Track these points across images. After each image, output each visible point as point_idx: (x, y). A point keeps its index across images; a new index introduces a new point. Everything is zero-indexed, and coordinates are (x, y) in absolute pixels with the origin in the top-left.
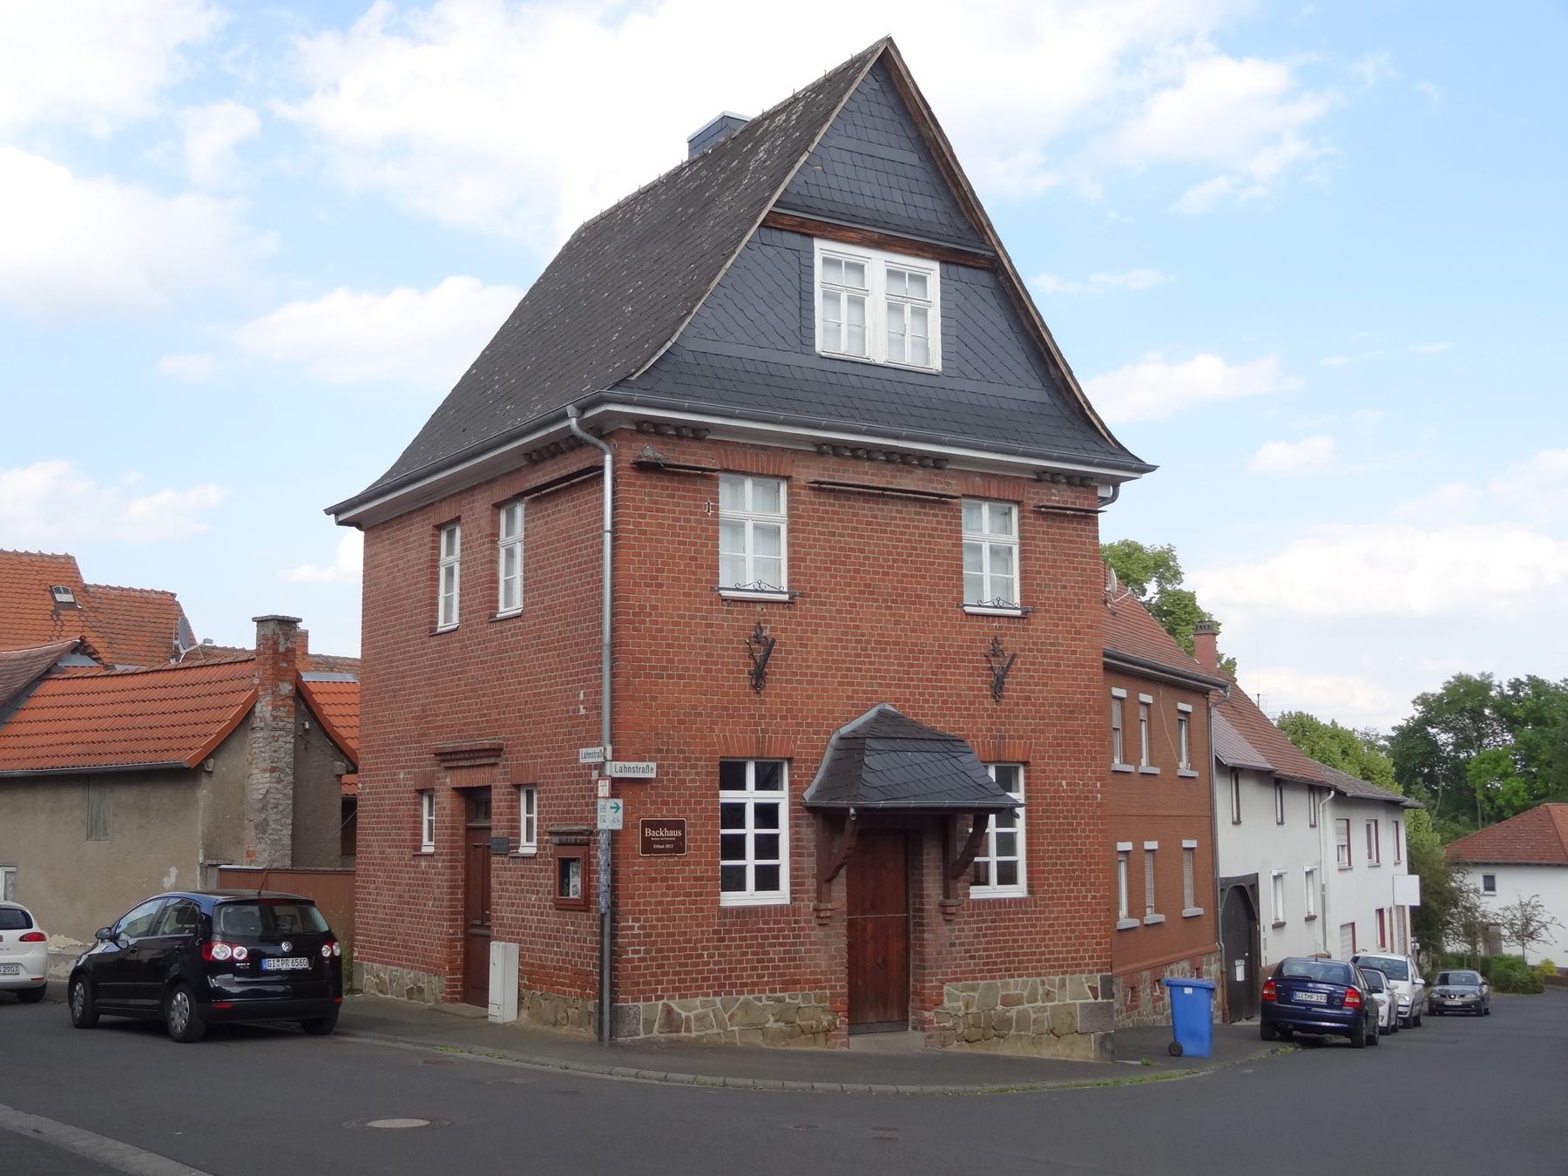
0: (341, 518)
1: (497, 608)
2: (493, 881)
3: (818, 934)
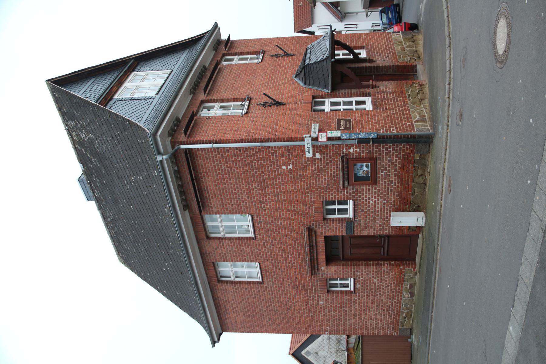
0: (216, 340)
1: (250, 238)
2: (365, 233)
3: (382, 88)
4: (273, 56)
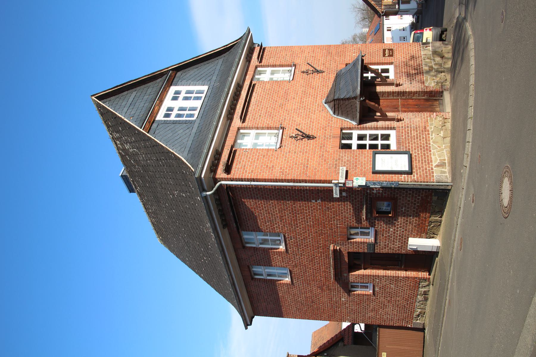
0: (249, 323)
2: (385, 251)
3: (406, 121)
4: (303, 72)
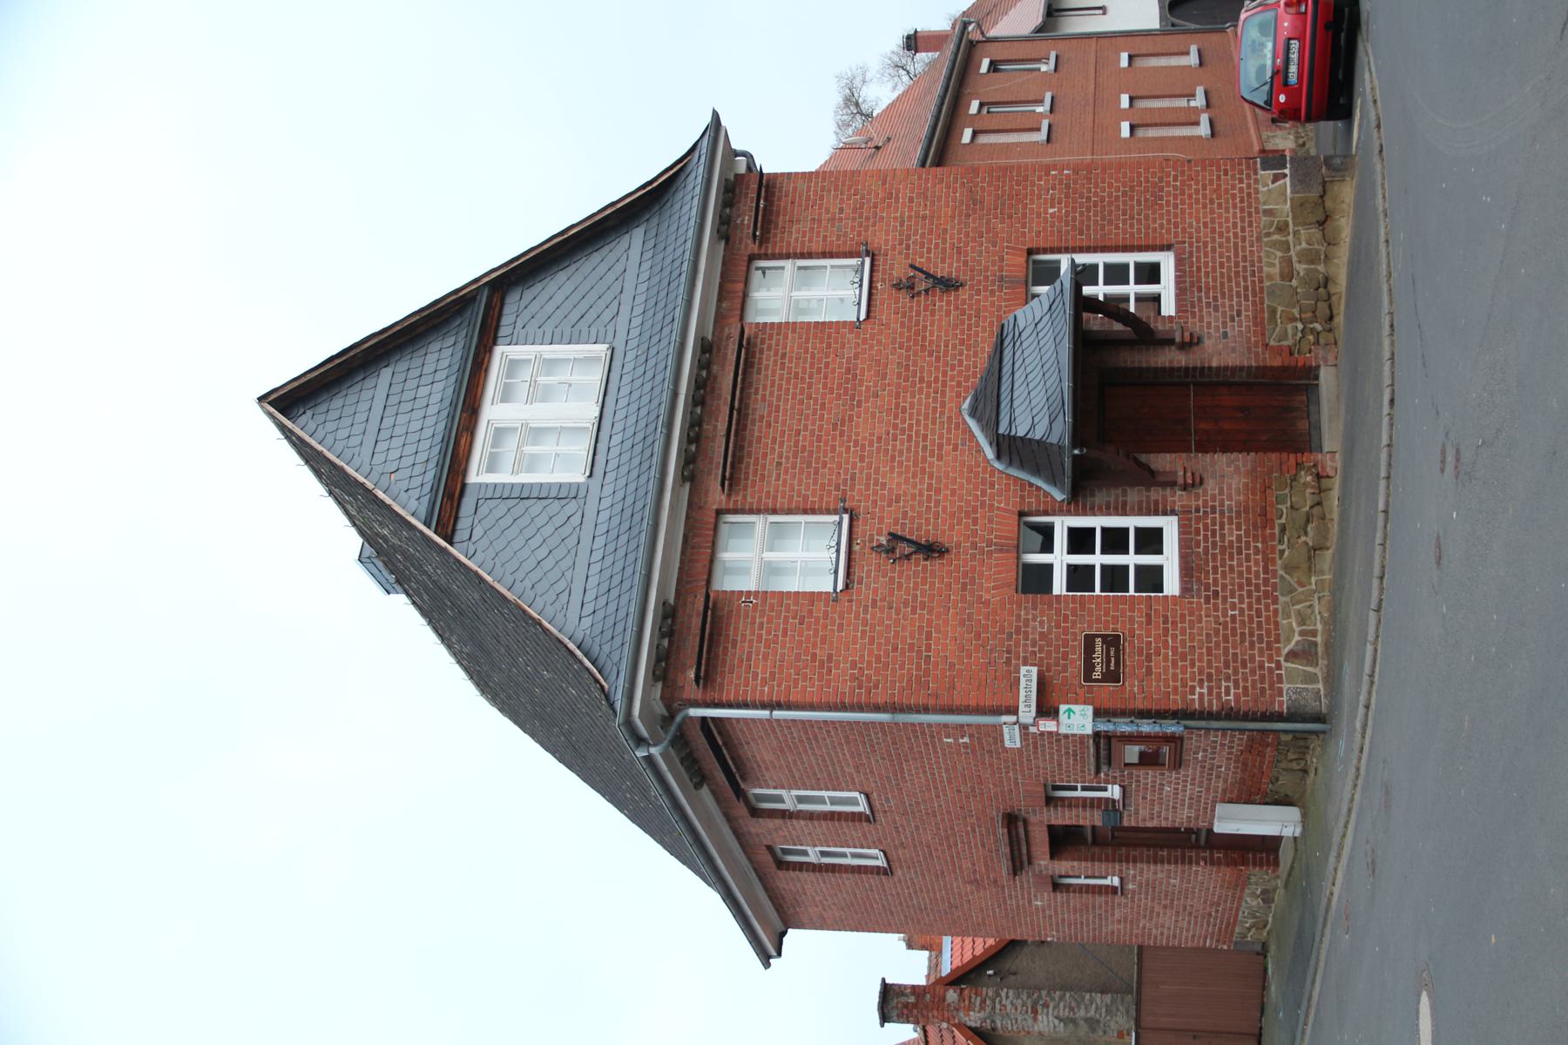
0: (774, 953)
1: (860, 814)
2: (1149, 824)
3: (1211, 486)
